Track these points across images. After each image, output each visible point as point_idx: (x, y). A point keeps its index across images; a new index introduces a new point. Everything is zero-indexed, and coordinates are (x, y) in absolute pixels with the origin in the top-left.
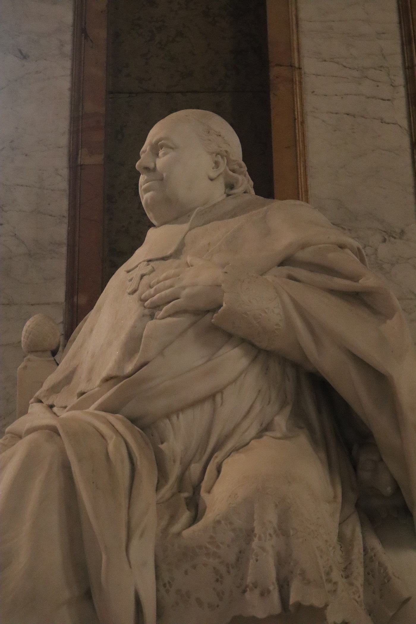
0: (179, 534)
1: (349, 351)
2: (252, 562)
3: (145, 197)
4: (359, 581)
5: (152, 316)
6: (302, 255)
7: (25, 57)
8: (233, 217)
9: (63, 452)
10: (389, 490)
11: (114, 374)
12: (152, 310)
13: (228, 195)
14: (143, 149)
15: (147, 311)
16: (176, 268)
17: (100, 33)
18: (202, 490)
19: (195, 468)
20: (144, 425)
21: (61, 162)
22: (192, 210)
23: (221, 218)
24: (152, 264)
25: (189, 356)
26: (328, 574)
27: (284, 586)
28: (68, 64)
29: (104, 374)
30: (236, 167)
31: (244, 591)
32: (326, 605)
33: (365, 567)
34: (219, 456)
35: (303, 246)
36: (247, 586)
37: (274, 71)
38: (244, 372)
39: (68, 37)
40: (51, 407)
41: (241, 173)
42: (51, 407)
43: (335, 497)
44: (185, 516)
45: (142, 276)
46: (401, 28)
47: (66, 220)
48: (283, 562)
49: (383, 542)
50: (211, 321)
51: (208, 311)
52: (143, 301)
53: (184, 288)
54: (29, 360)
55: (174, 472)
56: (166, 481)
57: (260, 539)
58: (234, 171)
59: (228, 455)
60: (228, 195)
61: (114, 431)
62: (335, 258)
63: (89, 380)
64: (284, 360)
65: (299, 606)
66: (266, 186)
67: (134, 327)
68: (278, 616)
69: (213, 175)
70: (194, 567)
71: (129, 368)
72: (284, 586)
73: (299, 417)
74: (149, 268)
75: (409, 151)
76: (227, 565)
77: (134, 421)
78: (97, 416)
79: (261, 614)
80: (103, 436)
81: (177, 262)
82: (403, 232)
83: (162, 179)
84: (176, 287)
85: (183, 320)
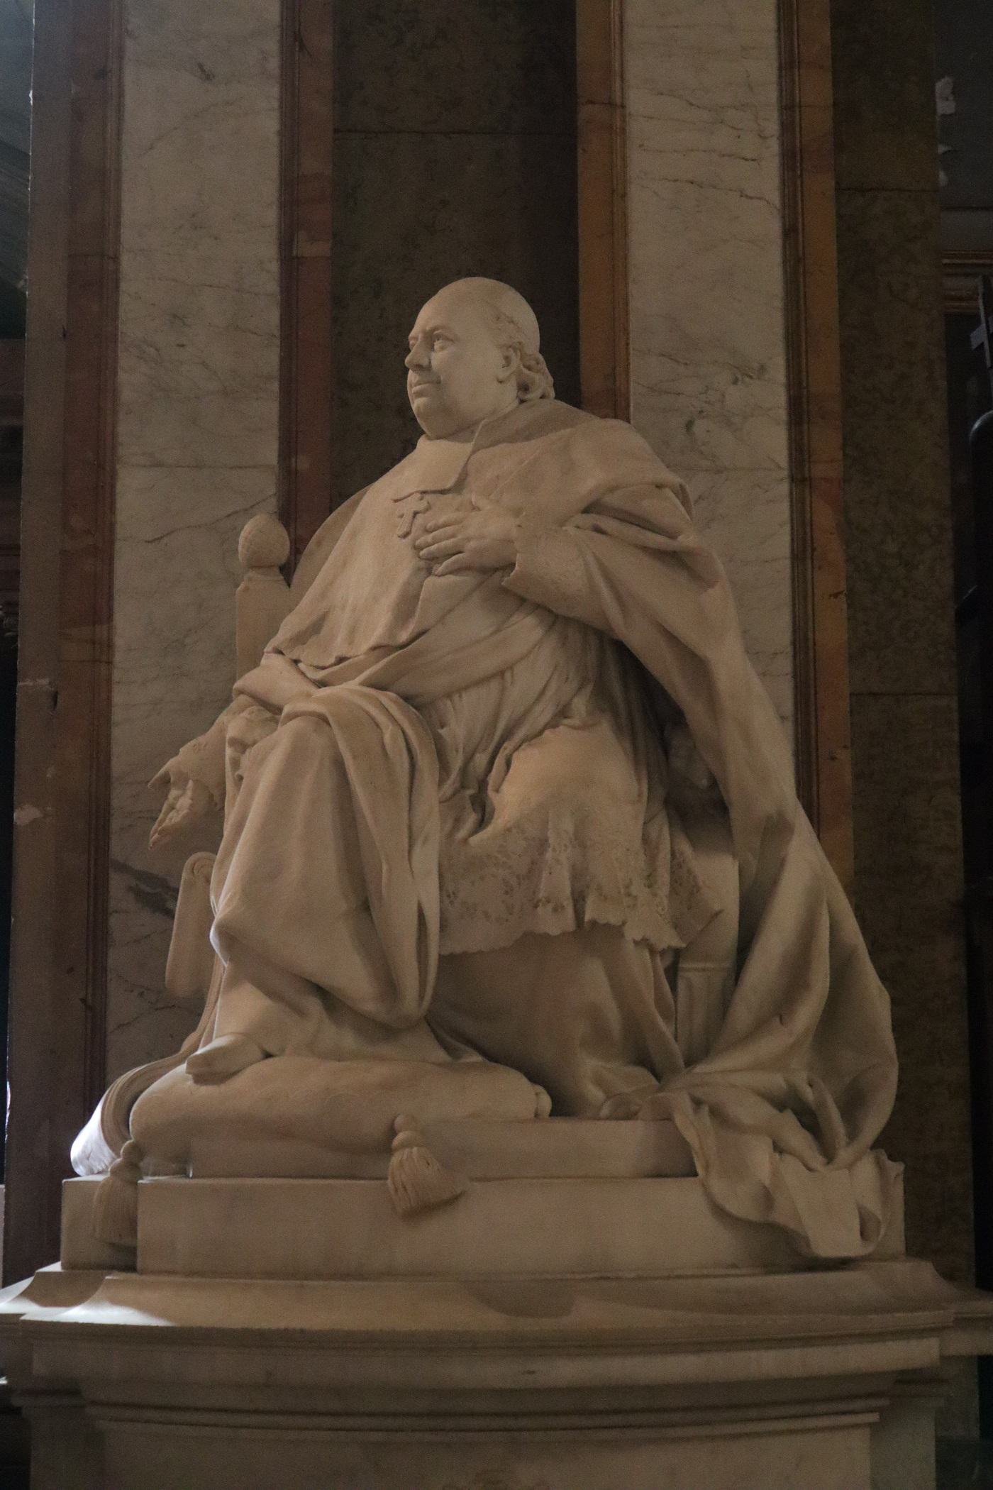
0: (465, 841)
1: (665, 630)
2: (545, 874)
3: (417, 404)
4: (664, 891)
5: (429, 572)
6: (614, 500)
7: (208, 76)
8: (528, 438)
9: (335, 745)
10: (704, 782)
11: (385, 642)
12: (429, 564)
13: (522, 401)
14: (412, 334)
15: (422, 564)
16: (458, 510)
17: (322, 42)
18: (490, 788)
19: (481, 760)
20: (419, 705)
21: (266, 251)
22: (476, 423)
23: (512, 439)
24: (427, 497)
25: (474, 623)
26: (627, 887)
27: (579, 900)
28: (275, 91)
29: (372, 641)
30: (533, 363)
31: (536, 906)
32: (624, 923)
33: (672, 873)
34: (509, 746)
35: (612, 489)
36: (539, 901)
37: (585, 112)
38: (539, 643)
39: (272, 45)
40: (296, 662)
41: (538, 371)
42: (296, 662)
43: (640, 795)
44: (471, 819)
45: (416, 514)
46: (779, 38)
47: (278, 342)
48: (577, 875)
49: (694, 845)
50: (498, 581)
51: (496, 570)
52: (418, 549)
53: (468, 539)
54: (250, 579)
55: (457, 762)
56: (448, 775)
57: (554, 850)
58: (529, 368)
59: (517, 749)
60: (522, 401)
61: (391, 721)
62: (651, 506)
63: (351, 639)
64: (585, 628)
65: (594, 923)
66: (570, 390)
67: (408, 583)
68: (574, 933)
69: (502, 374)
70: (482, 878)
71: (404, 636)
72: (579, 900)
73: (602, 695)
74: (423, 505)
75: (779, 242)
76: (518, 877)
77: (407, 698)
78: (363, 695)
79: (554, 931)
80: (377, 725)
81: (459, 499)
82: (762, 369)
83: (439, 382)
84: (460, 537)
85: (467, 580)
